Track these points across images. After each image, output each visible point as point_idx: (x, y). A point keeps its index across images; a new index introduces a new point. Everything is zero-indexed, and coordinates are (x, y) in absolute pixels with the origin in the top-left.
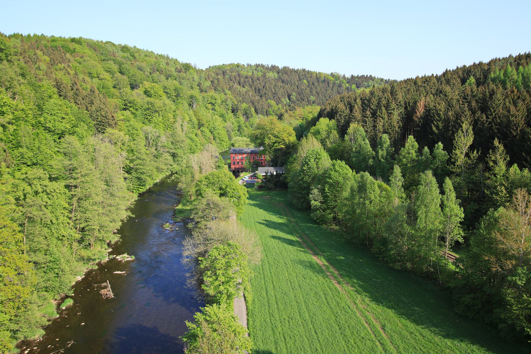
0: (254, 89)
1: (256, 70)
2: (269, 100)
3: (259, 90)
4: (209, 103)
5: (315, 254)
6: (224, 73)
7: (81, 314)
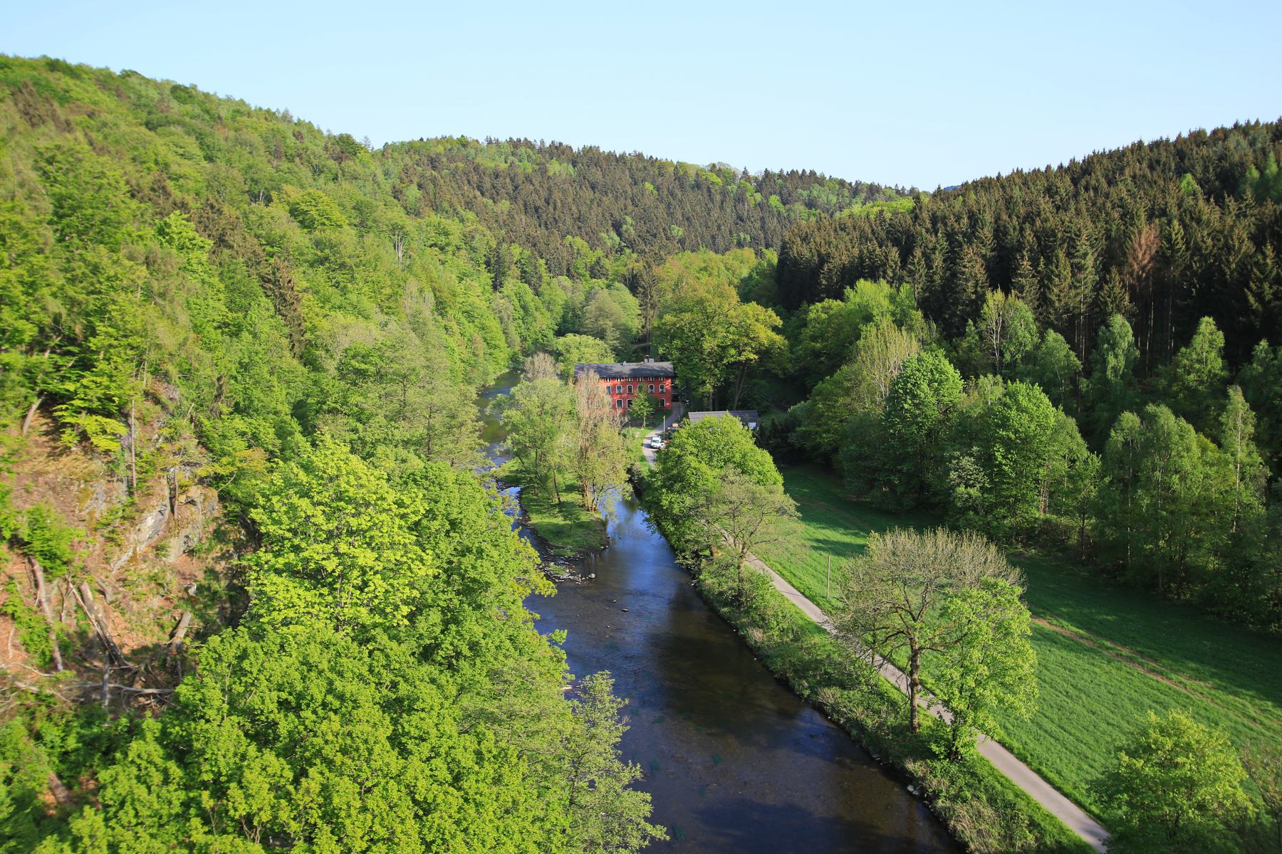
1: (513, 154)
3: (537, 209)
6: (434, 162)
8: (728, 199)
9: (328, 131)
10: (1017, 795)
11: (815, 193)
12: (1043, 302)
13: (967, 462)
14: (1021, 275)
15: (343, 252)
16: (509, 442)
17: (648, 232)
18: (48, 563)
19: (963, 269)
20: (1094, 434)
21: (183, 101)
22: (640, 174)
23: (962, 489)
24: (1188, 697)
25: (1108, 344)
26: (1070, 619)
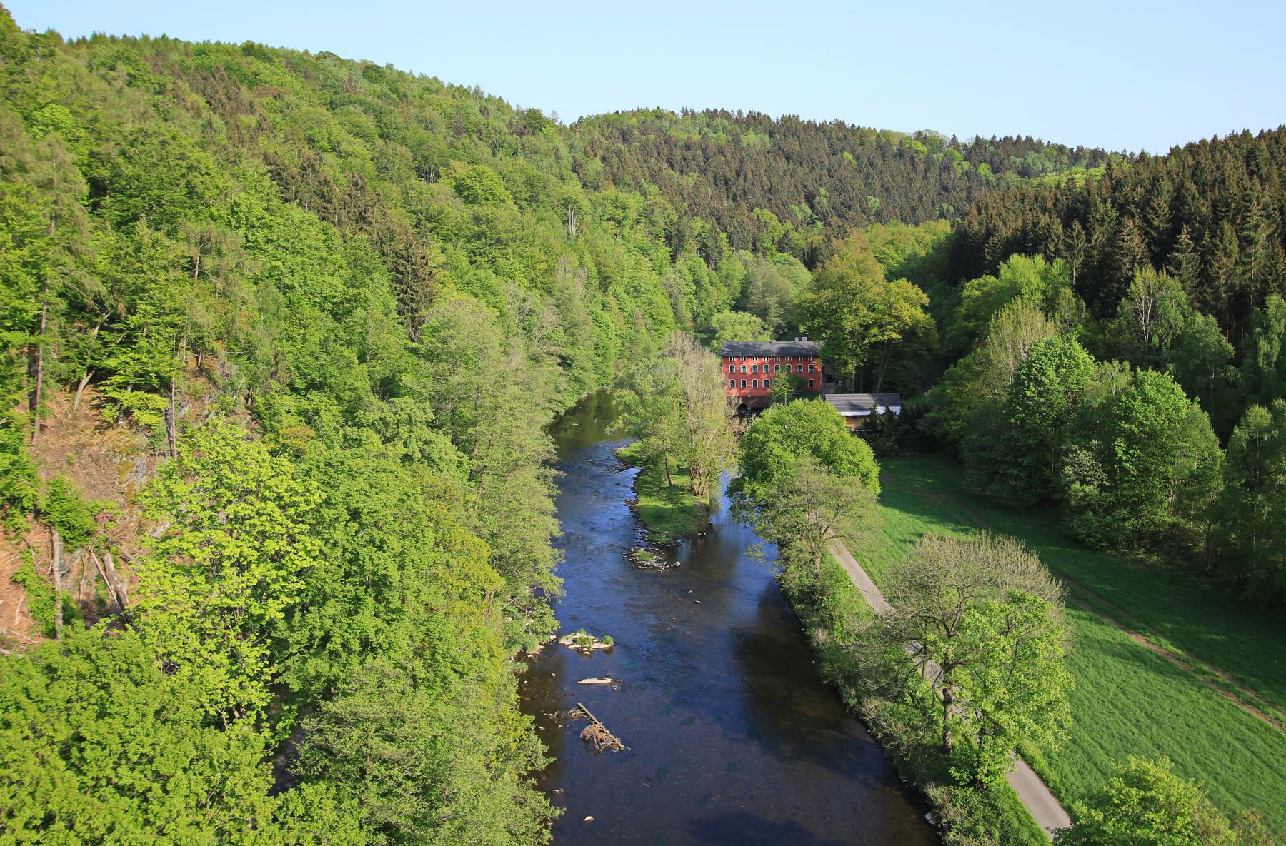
0: (712, 179)
1: (708, 125)
2: (757, 210)
3: (726, 181)
4: (608, 220)
5: (1128, 627)
6: (625, 136)
7: (565, 792)
8: (932, 168)
9: (518, 106)
10: (1032, 835)
11: (1030, 161)
12: (1205, 277)
13: (1084, 456)
14: (1177, 250)
15: (499, 228)
16: (620, 422)
17: (842, 203)
18: (68, 535)
19: (1121, 243)
20: (1223, 432)
21: (371, 80)
22: (839, 144)
23: (1077, 486)
24: (1279, 736)
25: (1262, 327)
26: (1173, 637)
